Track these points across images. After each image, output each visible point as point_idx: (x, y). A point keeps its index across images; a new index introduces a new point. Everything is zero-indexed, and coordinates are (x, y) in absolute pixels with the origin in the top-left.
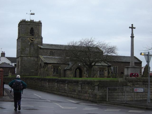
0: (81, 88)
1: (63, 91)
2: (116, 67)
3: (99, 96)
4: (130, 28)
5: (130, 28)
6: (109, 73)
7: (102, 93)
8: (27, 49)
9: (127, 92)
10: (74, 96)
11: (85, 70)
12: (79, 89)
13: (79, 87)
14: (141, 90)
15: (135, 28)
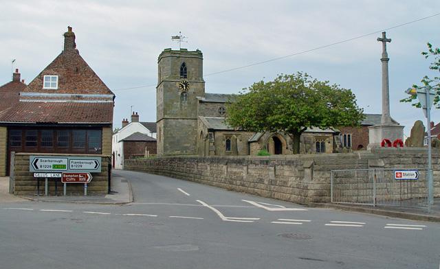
0: (275, 175)
1: (238, 182)
2: (349, 136)
3: (313, 192)
4: (379, 40)
5: (379, 40)
6: (335, 146)
7: (319, 185)
8: (175, 103)
9: (379, 181)
10: (259, 191)
11: (288, 141)
12: (271, 177)
13: (270, 173)
14: (410, 174)
15: (389, 41)
